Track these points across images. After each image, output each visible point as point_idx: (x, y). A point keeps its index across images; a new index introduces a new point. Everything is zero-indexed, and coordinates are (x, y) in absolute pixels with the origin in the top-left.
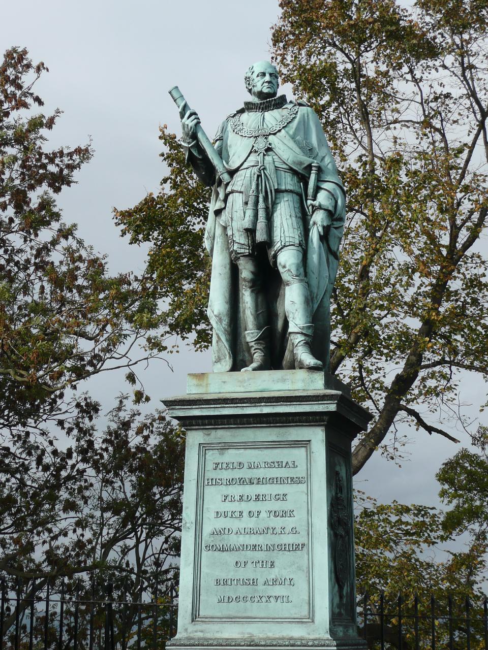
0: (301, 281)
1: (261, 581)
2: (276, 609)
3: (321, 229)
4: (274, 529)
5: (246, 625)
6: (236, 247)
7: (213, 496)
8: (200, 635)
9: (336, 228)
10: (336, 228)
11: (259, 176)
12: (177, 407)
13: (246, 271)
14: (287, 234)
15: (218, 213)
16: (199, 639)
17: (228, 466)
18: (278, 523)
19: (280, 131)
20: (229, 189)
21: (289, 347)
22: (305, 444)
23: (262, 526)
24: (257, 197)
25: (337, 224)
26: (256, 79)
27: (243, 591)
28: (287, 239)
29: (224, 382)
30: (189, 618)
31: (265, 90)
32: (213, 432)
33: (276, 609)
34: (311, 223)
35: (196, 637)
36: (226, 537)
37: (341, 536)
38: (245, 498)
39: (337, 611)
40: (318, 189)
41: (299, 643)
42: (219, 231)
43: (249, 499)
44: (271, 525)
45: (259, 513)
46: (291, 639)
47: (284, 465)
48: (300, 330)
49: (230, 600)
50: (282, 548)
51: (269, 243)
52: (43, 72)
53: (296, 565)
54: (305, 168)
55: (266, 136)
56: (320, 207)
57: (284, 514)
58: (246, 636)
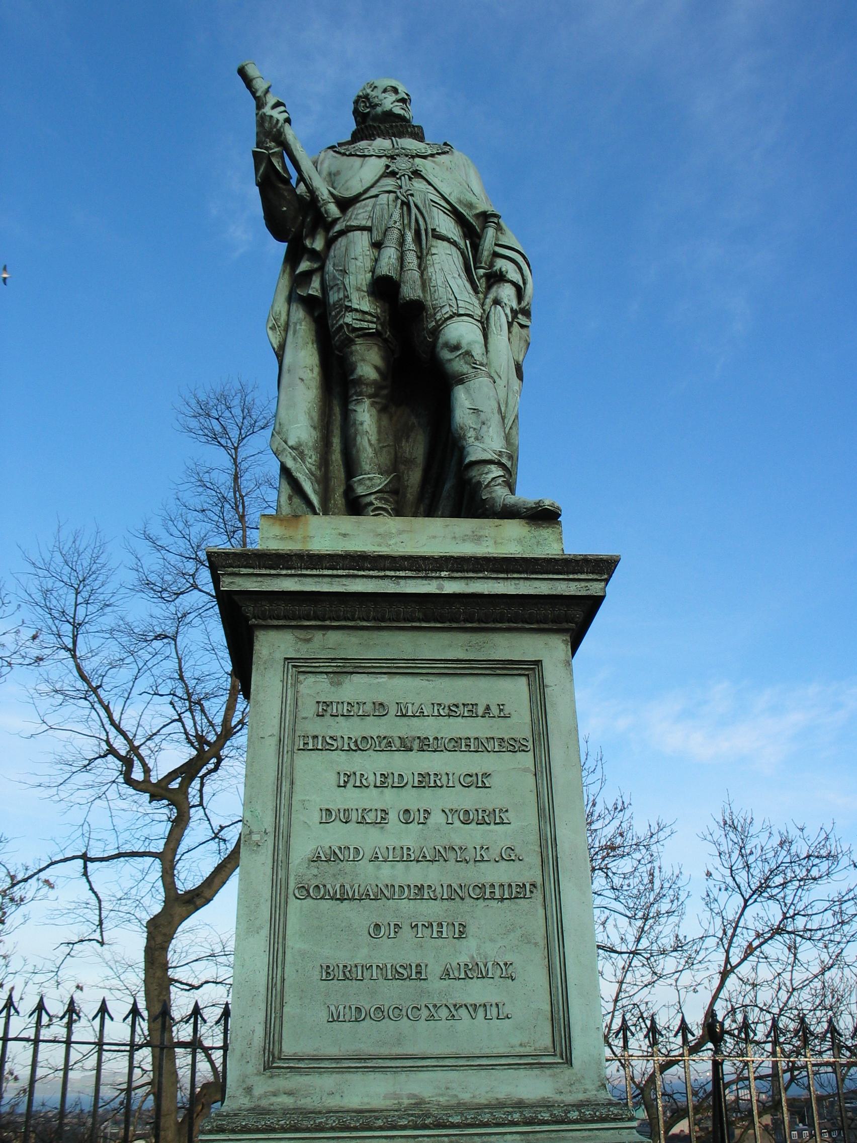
1: (435, 969)
5: (403, 1076)
12: (244, 571)
13: (368, 364)
16: (286, 1112)
17: (351, 711)
18: (471, 836)
24: (403, 236)
29: (345, 535)
30: (255, 1062)
32: (318, 636)
36: (347, 866)
44: (457, 841)
47: (480, 713)
48: (495, 457)
49: (359, 1016)
50: (484, 893)
53: (519, 932)
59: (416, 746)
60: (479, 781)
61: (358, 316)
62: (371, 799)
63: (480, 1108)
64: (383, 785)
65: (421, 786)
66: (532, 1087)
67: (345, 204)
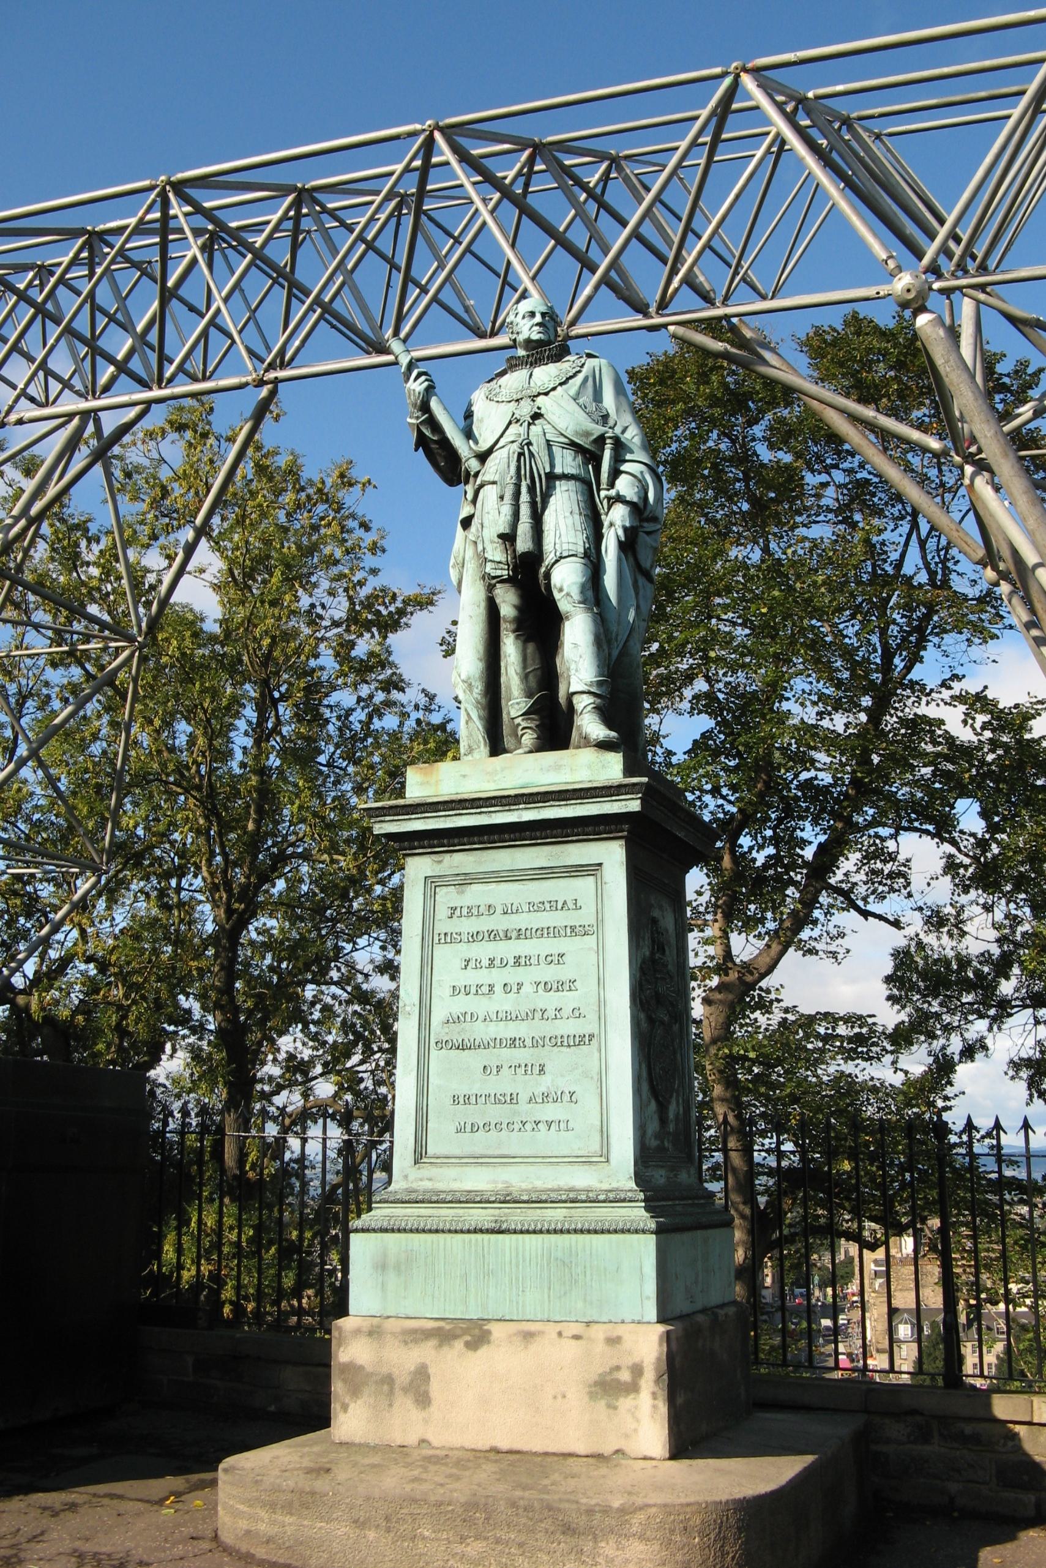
0: (590, 610)
1: (524, 1097)
2: (547, 1141)
3: (621, 532)
4: (544, 1011)
5: (500, 1169)
7: (447, 959)
8: (428, 1185)
9: (648, 533)
10: (648, 533)
11: (521, 455)
13: (508, 603)
14: (564, 539)
16: (425, 1192)
18: (549, 1001)
19: (554, 389)
20: (478, 482)
22: (593, 869)
23: (524, 1008)
24: (518, 487)
25: (649, 527)
26: (522, 322)
27: (495, 1113)
28: (565, 546)
31: (535, 336)
32: (447, 856)
33: (547, 1141)
34: (606, 524)
35: (421, 1188)
36: (467, 1026)
37: (662, 1023)
38: (497, 962)
39: (654, 1143)
40: (615, 473)
41: (584, 1197)
42: (470, 553)
43: (504, 964)
44: (541, 1005)
45: (520, 985)
46: (571, 1190)
49: (475, 1128)
50: (559, 1042)
52: (370, 489)
54: (595, 441)
55: (533, 398)
56: (619, 499)
57: (560, 986)
58: (500, 1186)
59: (514, 935)
61: (493, 565)
62: (484, 977)
66: (583, 1179)
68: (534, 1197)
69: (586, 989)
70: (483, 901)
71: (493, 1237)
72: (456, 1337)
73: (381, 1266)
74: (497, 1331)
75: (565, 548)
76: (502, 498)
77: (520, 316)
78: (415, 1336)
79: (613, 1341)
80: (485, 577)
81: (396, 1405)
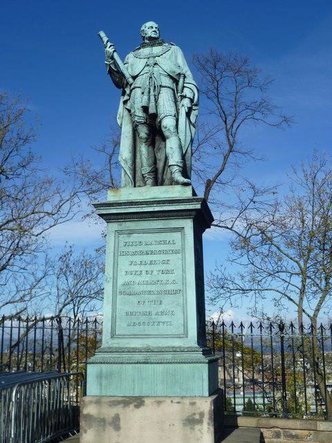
1: (154, 313)
6: (136, 119)
7: (124, 263)
13: (143, 132)
15: (125, 102)
16: (116, 348)
18: (164, 277)
20: (132, 87)
21: (169, 175)
23: (155, 279)
24: (150, 89)
27: (143, 319)
30: (109, 336)
32: (124, 224)
34: (181, 105)
44: (160, 279)
46: (173, 347)
48: (176, 164)
49: (134, 324)
50: (168, 293)
51: (155, 116)
56: (185, 97)
57: (168, 272)
59: (150, 253)
60: (167, 262)
62: (138, 268)
63: (176, 348)
64: (141, 264)
65: (151, 264)
66: (177, 343)
67: (134, 78)
68: (159, 350)
69: (178, 273)
70: (138, 240)
71: (145, 365)
72: (131, 403)
73: (100, 376)
74: (147, 401)
75: (168, 113)
76: (143, 93)
77: (147, 28)
78: (114, 403)
79: (193, 404)
80: (133, 122)
81: (107, 430)
